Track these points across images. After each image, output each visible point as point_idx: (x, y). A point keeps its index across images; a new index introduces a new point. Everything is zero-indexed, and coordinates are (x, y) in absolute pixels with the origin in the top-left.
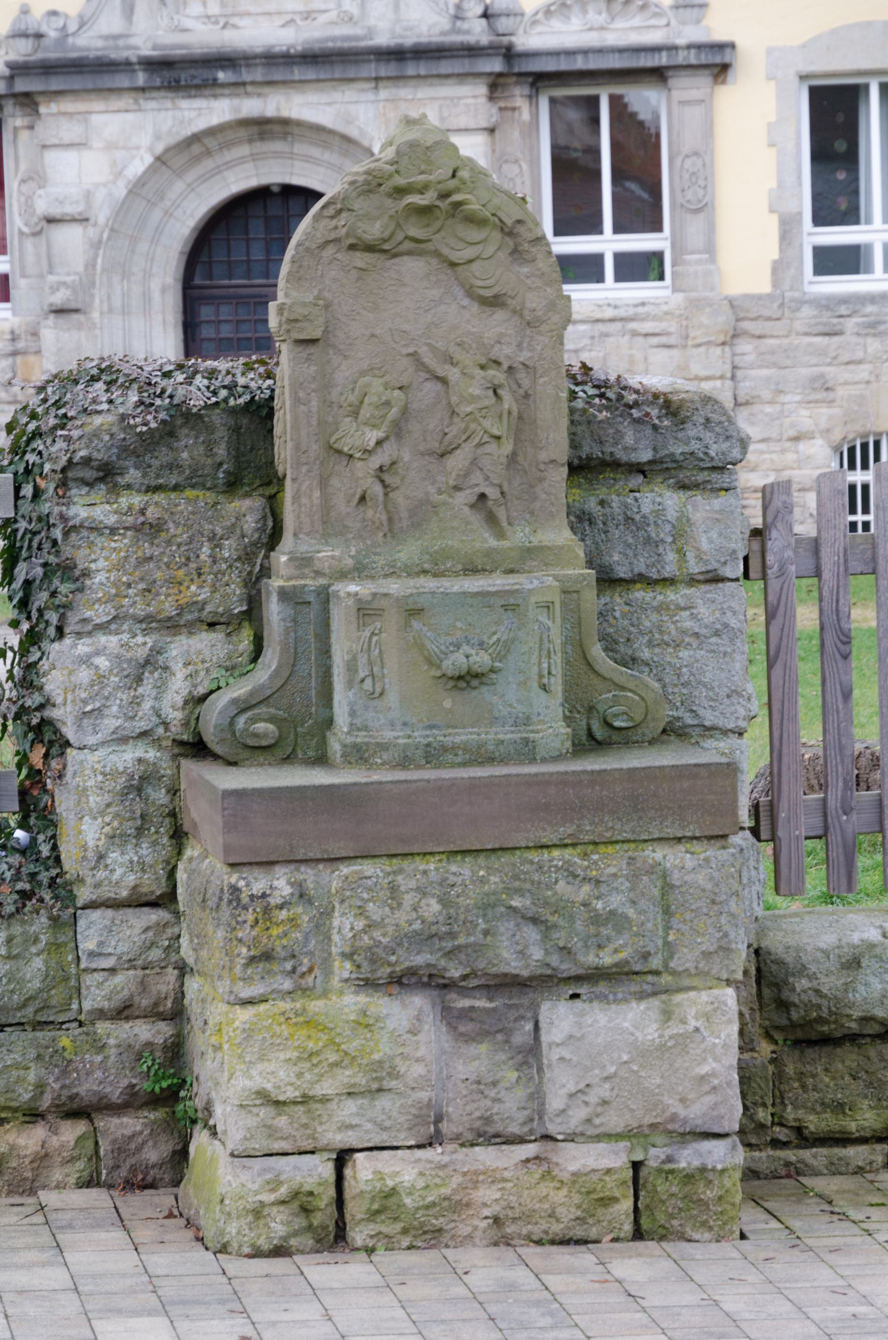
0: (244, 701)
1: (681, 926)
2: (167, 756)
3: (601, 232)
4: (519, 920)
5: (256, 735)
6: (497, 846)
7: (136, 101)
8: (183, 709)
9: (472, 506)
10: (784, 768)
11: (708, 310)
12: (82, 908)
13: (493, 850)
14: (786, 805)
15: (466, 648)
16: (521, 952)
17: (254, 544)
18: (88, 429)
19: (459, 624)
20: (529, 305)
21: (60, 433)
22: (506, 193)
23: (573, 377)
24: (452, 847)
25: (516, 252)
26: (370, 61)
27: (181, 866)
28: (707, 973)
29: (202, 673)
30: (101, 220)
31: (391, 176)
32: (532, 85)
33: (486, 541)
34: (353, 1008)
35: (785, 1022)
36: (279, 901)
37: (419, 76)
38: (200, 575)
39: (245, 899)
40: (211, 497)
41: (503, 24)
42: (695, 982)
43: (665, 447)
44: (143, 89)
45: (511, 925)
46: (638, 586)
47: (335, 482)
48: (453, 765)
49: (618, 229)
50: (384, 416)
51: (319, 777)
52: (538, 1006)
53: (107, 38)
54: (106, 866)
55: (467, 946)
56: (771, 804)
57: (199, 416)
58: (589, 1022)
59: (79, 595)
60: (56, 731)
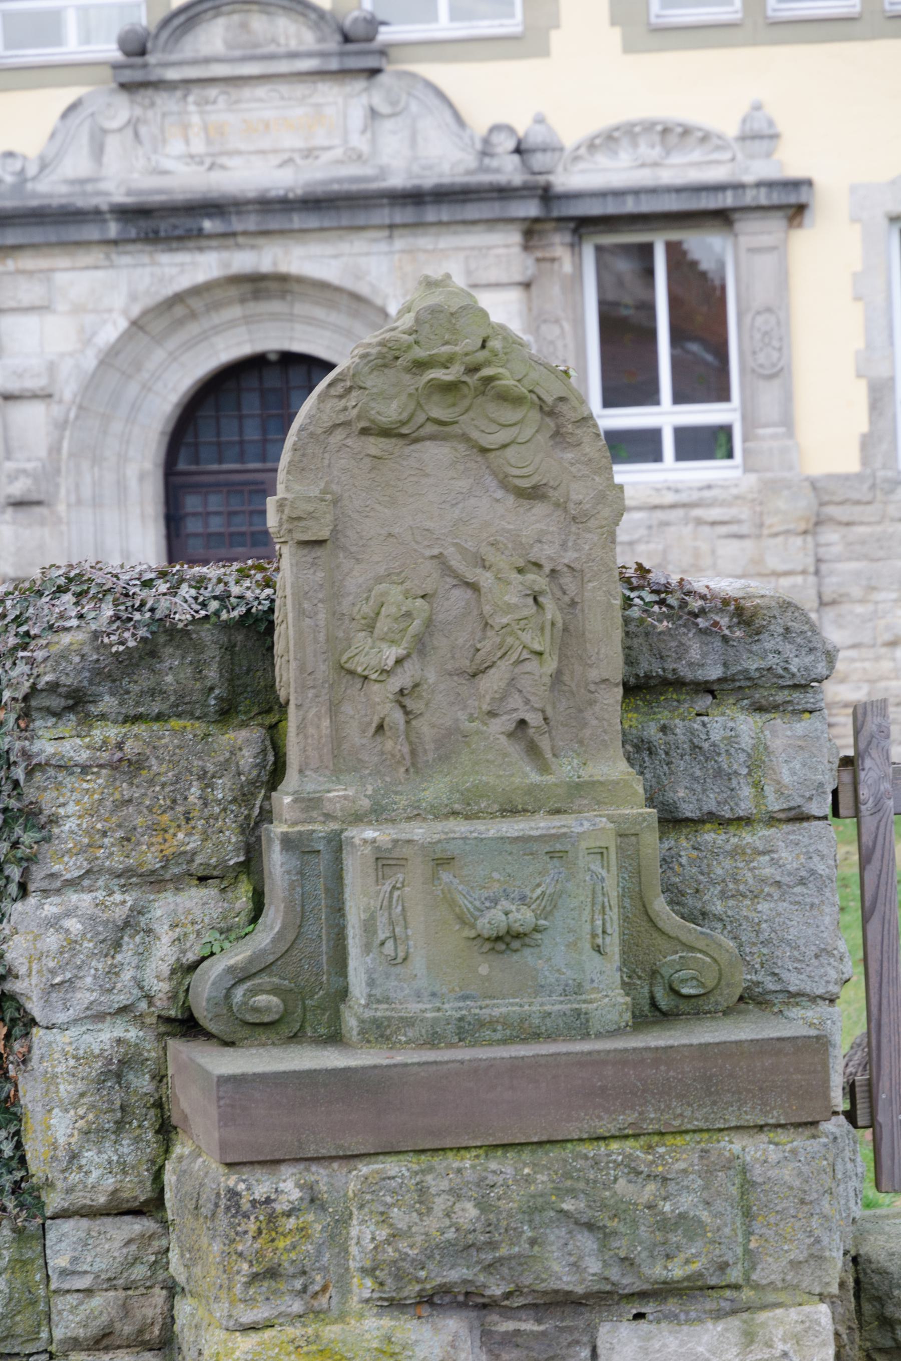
0: (243, 969)
1: (764, 1230)
2: (151, 1036)
3: (657, 402)
4: (572, 1226)
5: (256, 1010)
6: (544, 1138)
7: (108, 257)
8: (170, 979)
9: (510, 735)
10: (884, 1041)
11: (786, 493)
12: (52, 1218)
13: (540, 1143)
14: (887, 1084)
15: (504, 904)
16: (574, 1264)
17: (252, 783)
18: (54, 649)
19: (496, 875)
20: (574, 497)
21: (21, 654)
22: (546, 366)
23: (627, 581)
24: (491, 1141)
25: (558, 435)
26: (382, 206)
27: (169, 1166)
28: (796, 1287)
29: (192, 937)
30: (68, 395)
31: (409, 347)
32: (575, 231)
33: (526, 775)
34: (376, 1333)
35: (889, 1343)
36: (286, 1207)
37: (440, 223)
38: (188, 820)
39: (246, 1206)
40: (200, 727)
41: (538, 161)
42: (782, 1297)
43: (737, 662)
44: (115, 242)
45: (563, 1232)
46: (708, 826)
47: (347, 708)
48: (491, 1043)
49: (679, 398)
50: (404, 630)
51: (332, 1059)
52: (596, 1328)
53: (72, 182)
54: (80, 1167)
55: (510, 1258)
56: (869, 1083)
57: (185, 632)
58: (657, 1346)
59: (46, 846)
60: (20, 1007)
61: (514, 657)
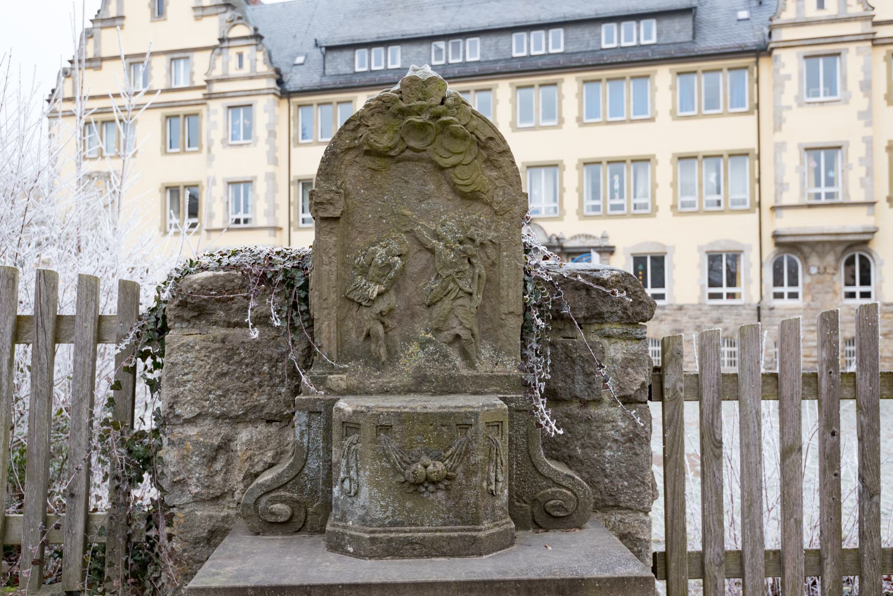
5: (273, 514)
38: (260, 387)
61: (454, 295)
